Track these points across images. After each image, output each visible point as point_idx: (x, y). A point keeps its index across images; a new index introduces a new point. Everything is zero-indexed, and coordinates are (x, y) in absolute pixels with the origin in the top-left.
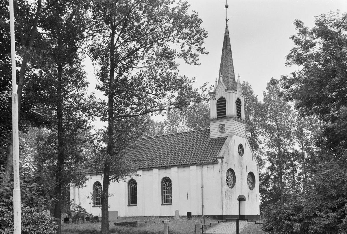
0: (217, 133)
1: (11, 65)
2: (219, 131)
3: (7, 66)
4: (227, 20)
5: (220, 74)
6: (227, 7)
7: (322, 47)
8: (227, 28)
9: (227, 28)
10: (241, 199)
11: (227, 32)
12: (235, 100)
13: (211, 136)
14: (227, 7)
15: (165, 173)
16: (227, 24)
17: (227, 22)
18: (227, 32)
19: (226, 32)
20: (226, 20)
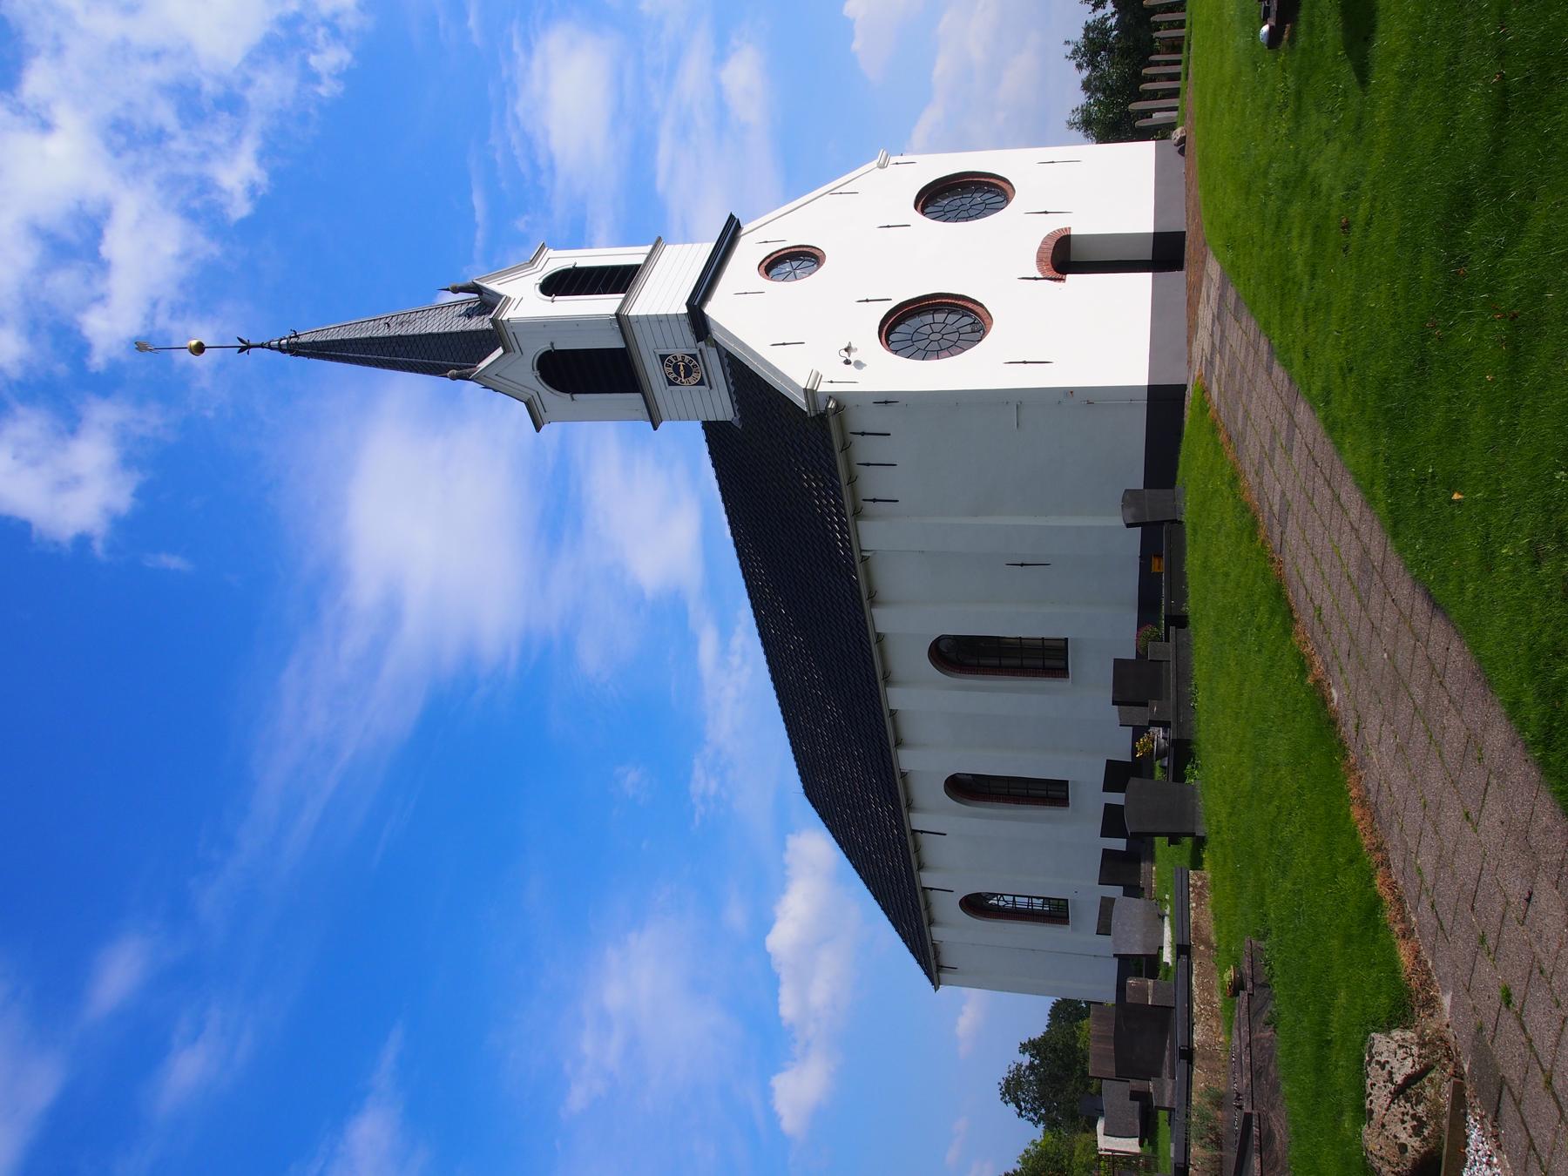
0: (714, 392)
2: (701, 383)
11: (295, 349)
20: (242, 350)
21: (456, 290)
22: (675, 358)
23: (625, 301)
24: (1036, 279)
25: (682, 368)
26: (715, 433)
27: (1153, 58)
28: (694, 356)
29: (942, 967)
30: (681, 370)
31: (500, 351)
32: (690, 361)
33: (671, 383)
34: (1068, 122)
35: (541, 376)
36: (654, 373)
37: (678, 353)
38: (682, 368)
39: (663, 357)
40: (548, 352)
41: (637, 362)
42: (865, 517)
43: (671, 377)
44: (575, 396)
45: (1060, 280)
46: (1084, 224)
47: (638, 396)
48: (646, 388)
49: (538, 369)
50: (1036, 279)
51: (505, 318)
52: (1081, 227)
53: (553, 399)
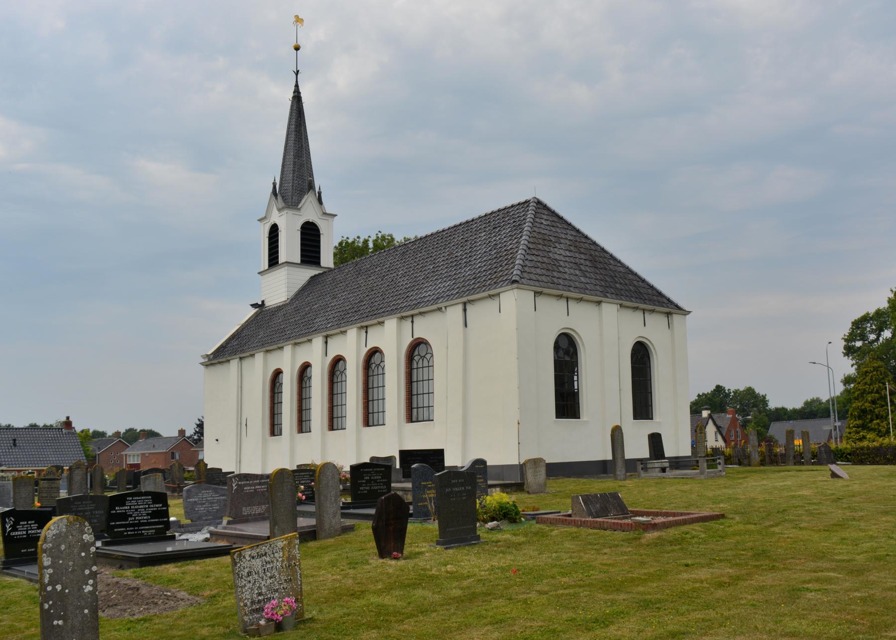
6: (297, 48)
8: (297, 86)
9: (297, 86)
11: (297, 98)
14: (297, 48)
16: (297, 81)
41: (275, 268)
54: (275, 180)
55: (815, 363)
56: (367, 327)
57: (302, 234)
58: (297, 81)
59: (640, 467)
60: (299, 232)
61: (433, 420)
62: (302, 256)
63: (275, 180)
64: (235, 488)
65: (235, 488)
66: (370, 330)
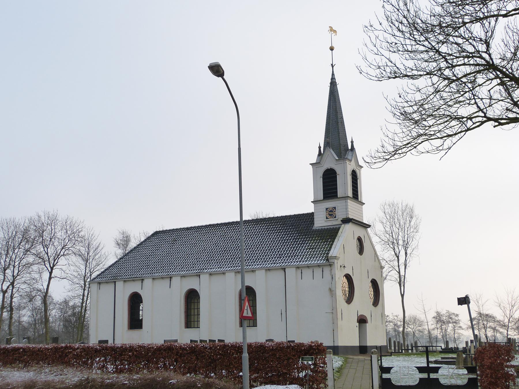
0: (324, 221)
1: (91, 367)
2: (327, 218)
3: (285, 382)
4: (332, 66)
5: (241, 310)
6: (332, 49)
7: (479, 74)
8: (333, 74)
9: (333, 74)
10: (362, 321)
11: (333, 84)
12: (349, 172)
13: (315, 225)
14: (332, 49)
15: (134, 287)
16: (333, 72)
17: (333, 67)
18: (333, 84)
19: (332, 79)
20: (332, 65)
21: (352, 142)
22: (335, 212)
23: (350, 198)
24: (358, 315)
25: (332, 213)
26: (309, 217)
27: (350, 148)
28: (335, 217)
29: (100, 284)
30: (331, 213)
31: (337, 158)
32: (328, 211)
33: (327, 209)
34: (438, 313)
35: (328, 169)
36: (330, 204)
37: (336, 213)
38: (332, 213)
39: (335, 208)
40: (336, 173)
41: (333, 200)
42: (296, 270)
43: (328, 209)
44: (322, 178)
45: (357, 321)
46: (369, 326)
47: (322, 198)
48: (324, 201)
49: (330, 168)
50: (358, 315)
51: (347, 162)
52: (368, 325)
53: (321, 171)
54: (320, 145)
55: (281, 314)
56: (100, 283)
57: (324, 179)
58: (333, 72)
59: (385, 376)
60: (322, 179)
61: (199, 328)
62: (324, 194)
63: (320, 145)
64: (98, 359)
65: (98, 359)
66: (101, 284)
